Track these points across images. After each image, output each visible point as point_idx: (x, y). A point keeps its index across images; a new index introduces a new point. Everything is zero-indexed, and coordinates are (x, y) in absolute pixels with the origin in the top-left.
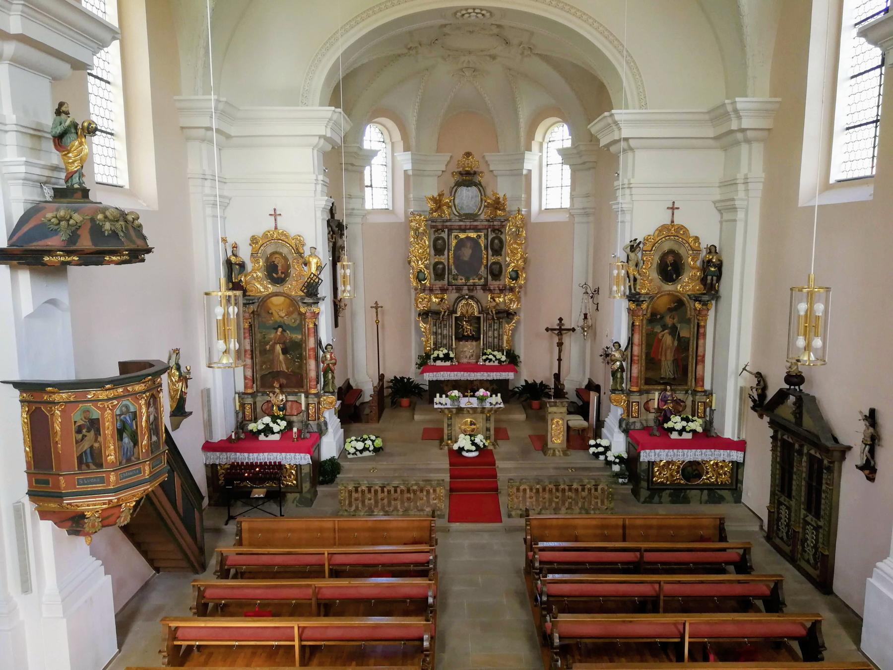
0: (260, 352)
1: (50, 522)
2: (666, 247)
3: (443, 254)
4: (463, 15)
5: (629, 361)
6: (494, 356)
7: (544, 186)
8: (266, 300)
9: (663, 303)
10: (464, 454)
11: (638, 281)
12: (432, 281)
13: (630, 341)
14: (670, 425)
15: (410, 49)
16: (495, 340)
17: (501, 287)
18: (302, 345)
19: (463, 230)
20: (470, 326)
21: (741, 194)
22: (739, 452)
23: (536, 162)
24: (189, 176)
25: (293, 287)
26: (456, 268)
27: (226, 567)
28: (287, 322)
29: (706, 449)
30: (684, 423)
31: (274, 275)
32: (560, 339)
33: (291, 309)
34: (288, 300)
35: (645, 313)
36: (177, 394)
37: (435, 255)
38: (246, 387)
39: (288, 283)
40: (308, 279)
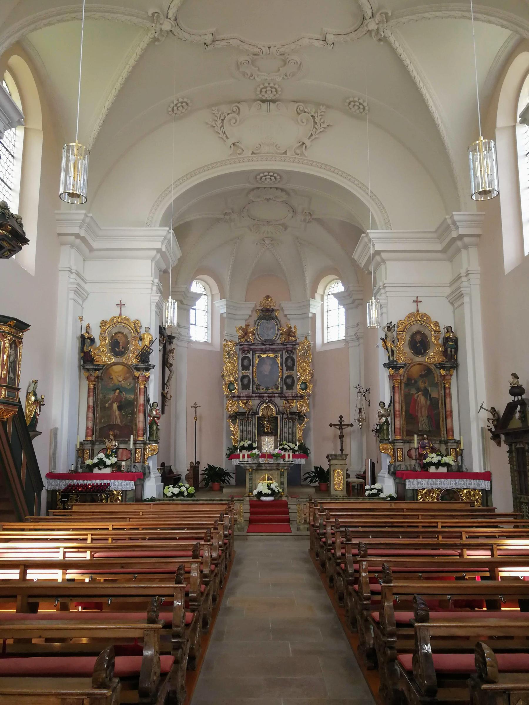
0: (101, 408)
2: (415, 329)
4: (261, 178)
5: (393, 416)
6: (289, 446)
7: (325, 326)
8: (109, 368)
9: (415, 371)
10: (263, 498)
11: (395, 352)
12: (240, 390)
13: (392, 399)
14: (428, 460)
15: (225, 214)
16: (290, 436)
17: (294, 394)
18: (134, 403)
19: (264, 352)
20: (270, 424)
21: (465, 284)
22: (487, 482)
24: (60, 269)
25: (132, 359)
28: (123, 386)
29: (460, 479)
30: (440, 458)
31: (117, 349)
32: (341, 432)
33: (128, 375)
34: (125, 368)
35: (402, 378)
36: (31, 414)
37: (243, 370)
38: (87, 436)
39: (126, 355)
40: (142, 350)
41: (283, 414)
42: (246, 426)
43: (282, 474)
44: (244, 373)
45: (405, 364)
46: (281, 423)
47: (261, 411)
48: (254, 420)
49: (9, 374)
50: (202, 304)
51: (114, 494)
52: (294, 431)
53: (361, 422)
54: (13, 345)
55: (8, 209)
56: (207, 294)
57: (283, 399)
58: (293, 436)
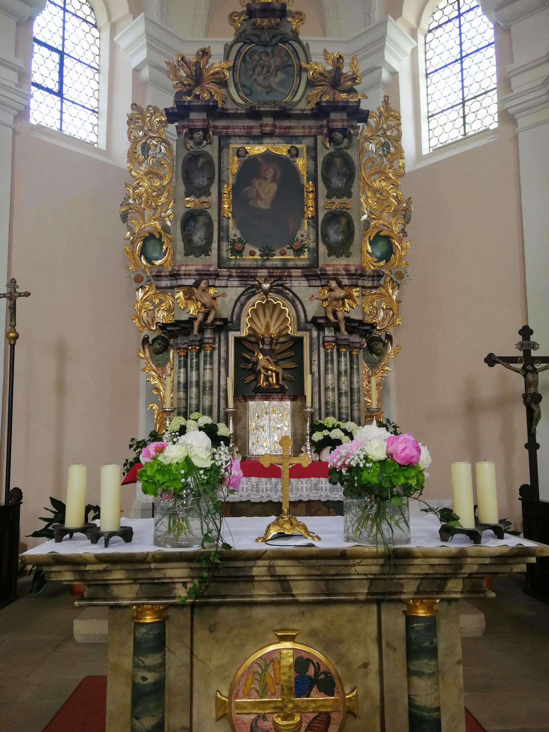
16: (344, 399)
17: (353, 269)
19: (258, 139)
20: (276, 364)
26: (239, 226)
27: (338, 470)
41: (320, 328)
42: (198, 369)
44: (191, 202)
46: (315, 358)
47: (245, 320)
48: (223, 349)
52: (355, 386)
58: (352, 402)
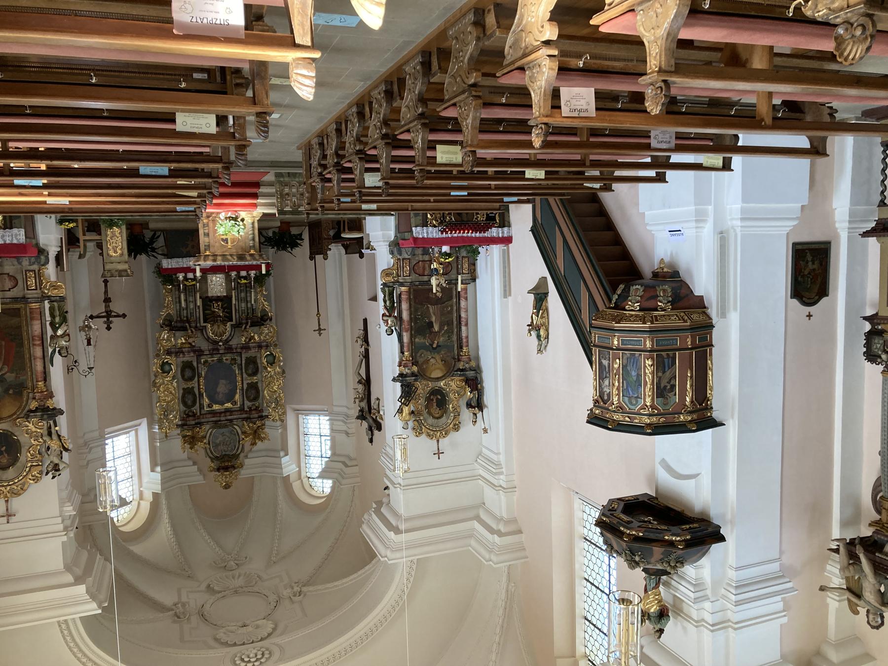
1: (696, 294)
3: (248, 384)
4: (263, 654)
11: (45, 433)
12: (259, 355)
17: (181, 356)
19: (227, 411)
20: (214, 312)
23: (145, 480)
25: (422, 388)
31: (439, 397)
35: (31, 395)
36: (542, 314)
41: (196, 327)
43: (208, 247)
44: (255, 379)
45: (27, 417)
46: (198, 315)
47: (229, 329)
48: (238, 316)
49: (609, 364)
50: (315, 466)
51: (436, 221)
53: (87, 326)
54: (606, 398)
55: (627, 560)
56: (306, 479)
57: (197, 348)
